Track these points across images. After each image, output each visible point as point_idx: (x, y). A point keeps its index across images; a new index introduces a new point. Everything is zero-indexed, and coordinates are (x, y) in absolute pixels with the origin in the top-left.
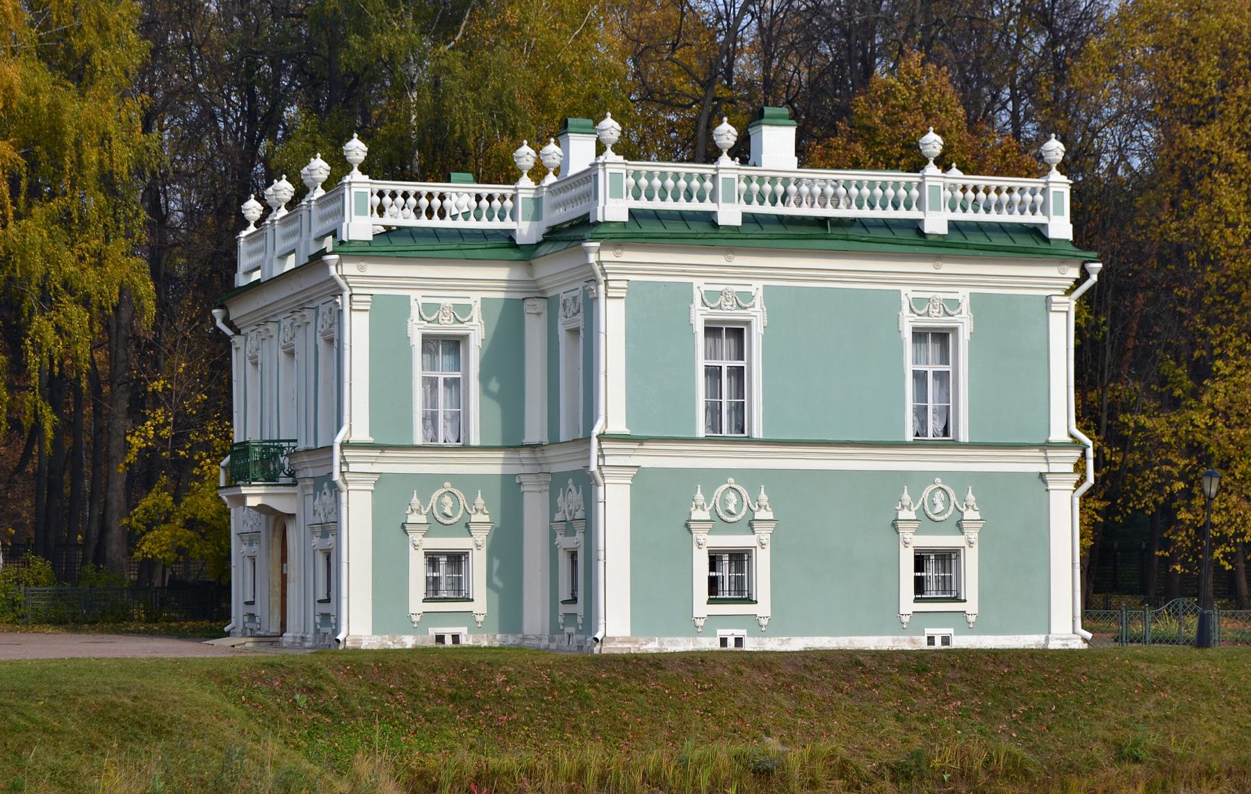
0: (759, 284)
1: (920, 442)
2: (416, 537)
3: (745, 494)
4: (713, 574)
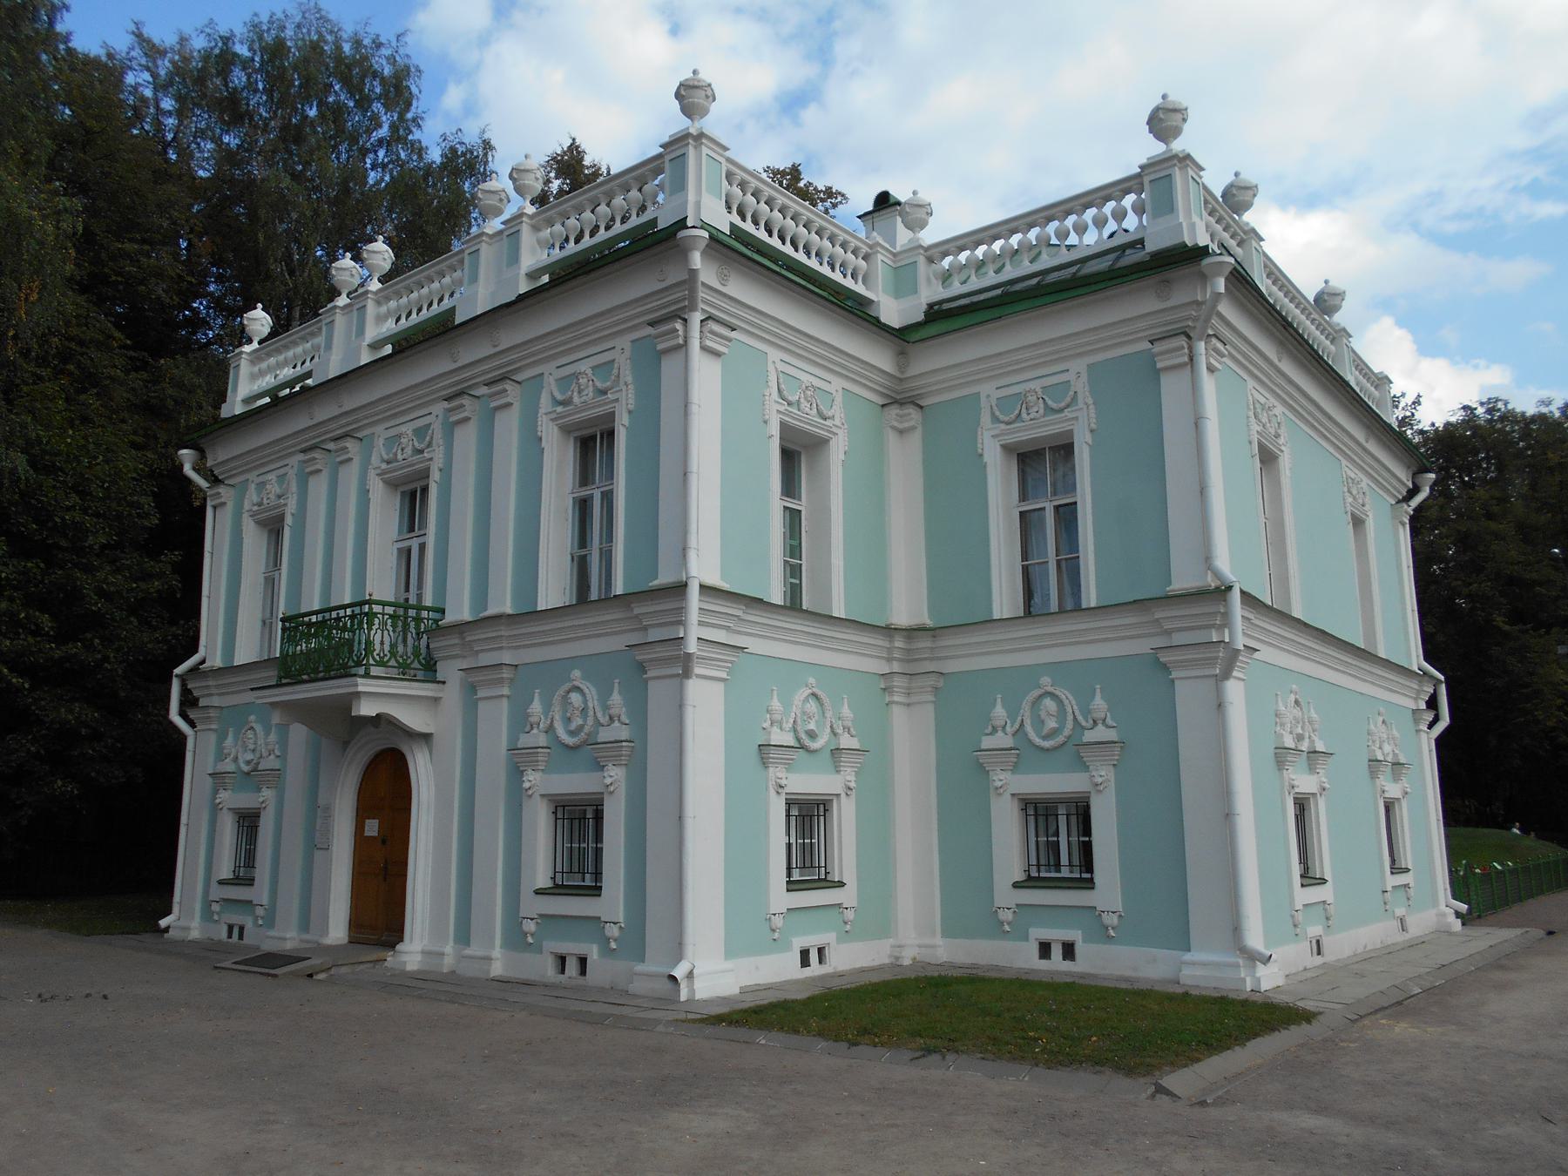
0: (1079, 365)
2: (1000, 777)
3: (826, 701)
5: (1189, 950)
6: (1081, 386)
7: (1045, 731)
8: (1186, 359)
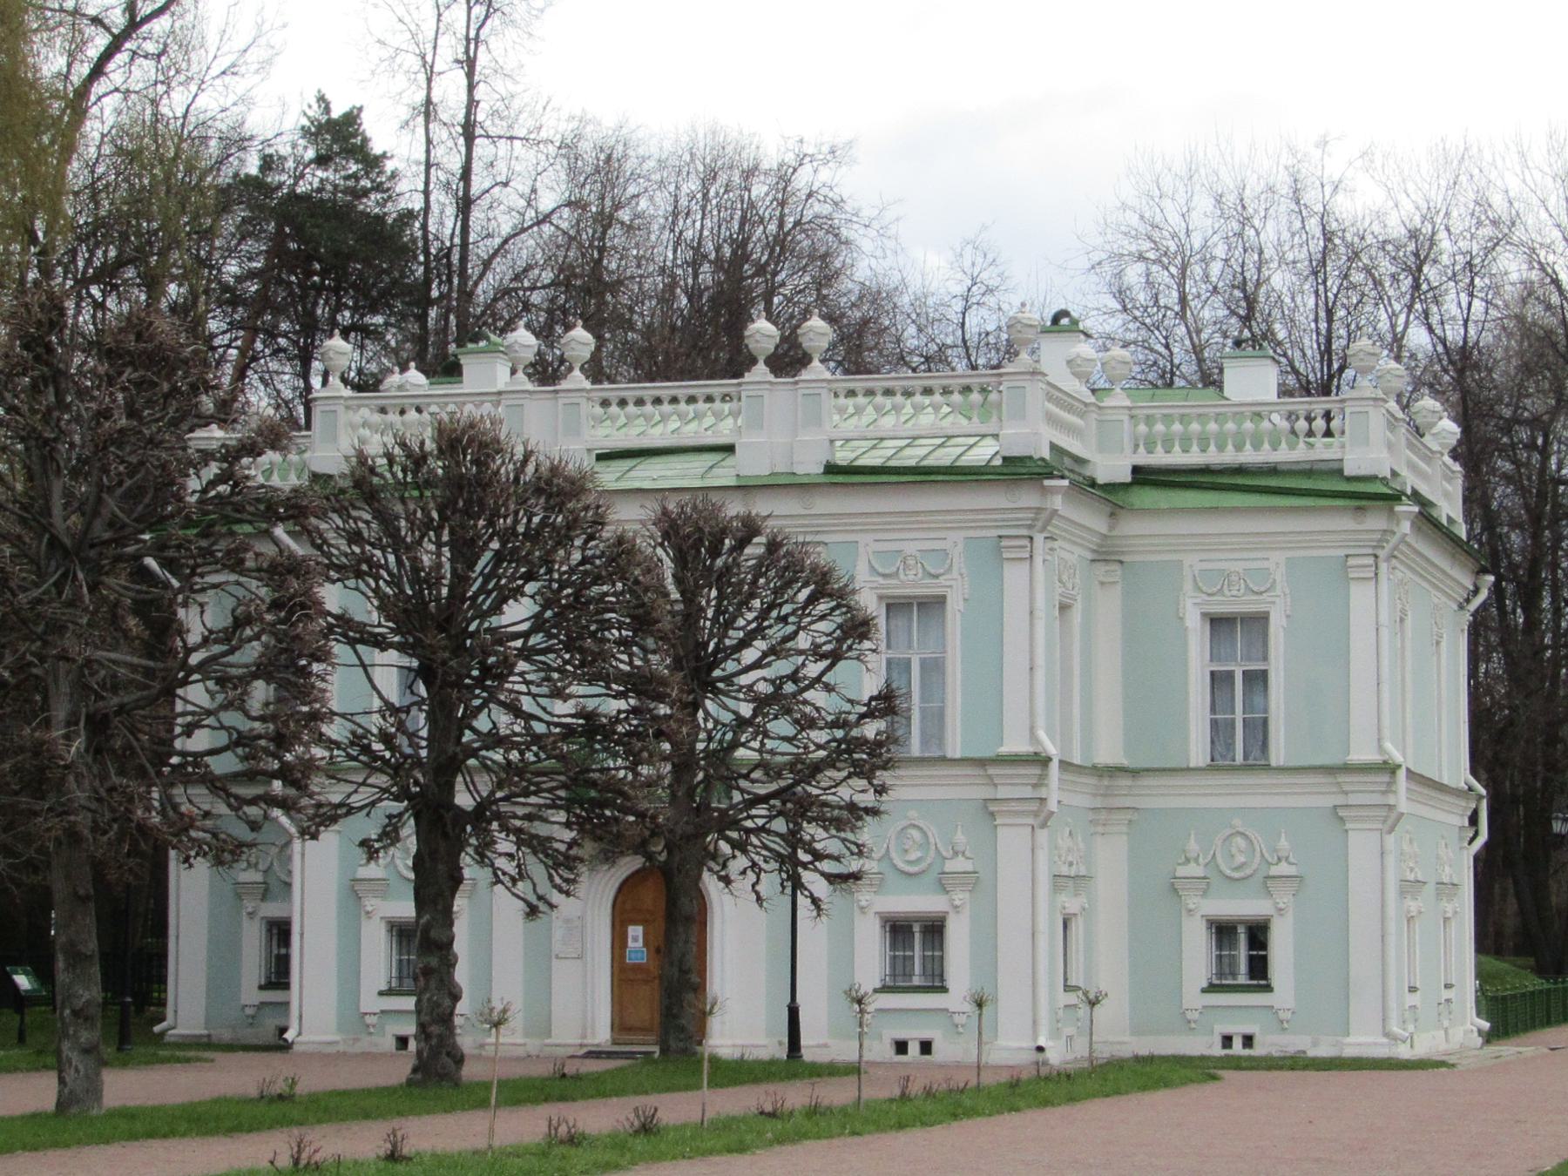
2: (1192, 901)
3: (933, 832)
5: (1348, 1035)
6: (1279, 576)
8: (1372, 575)
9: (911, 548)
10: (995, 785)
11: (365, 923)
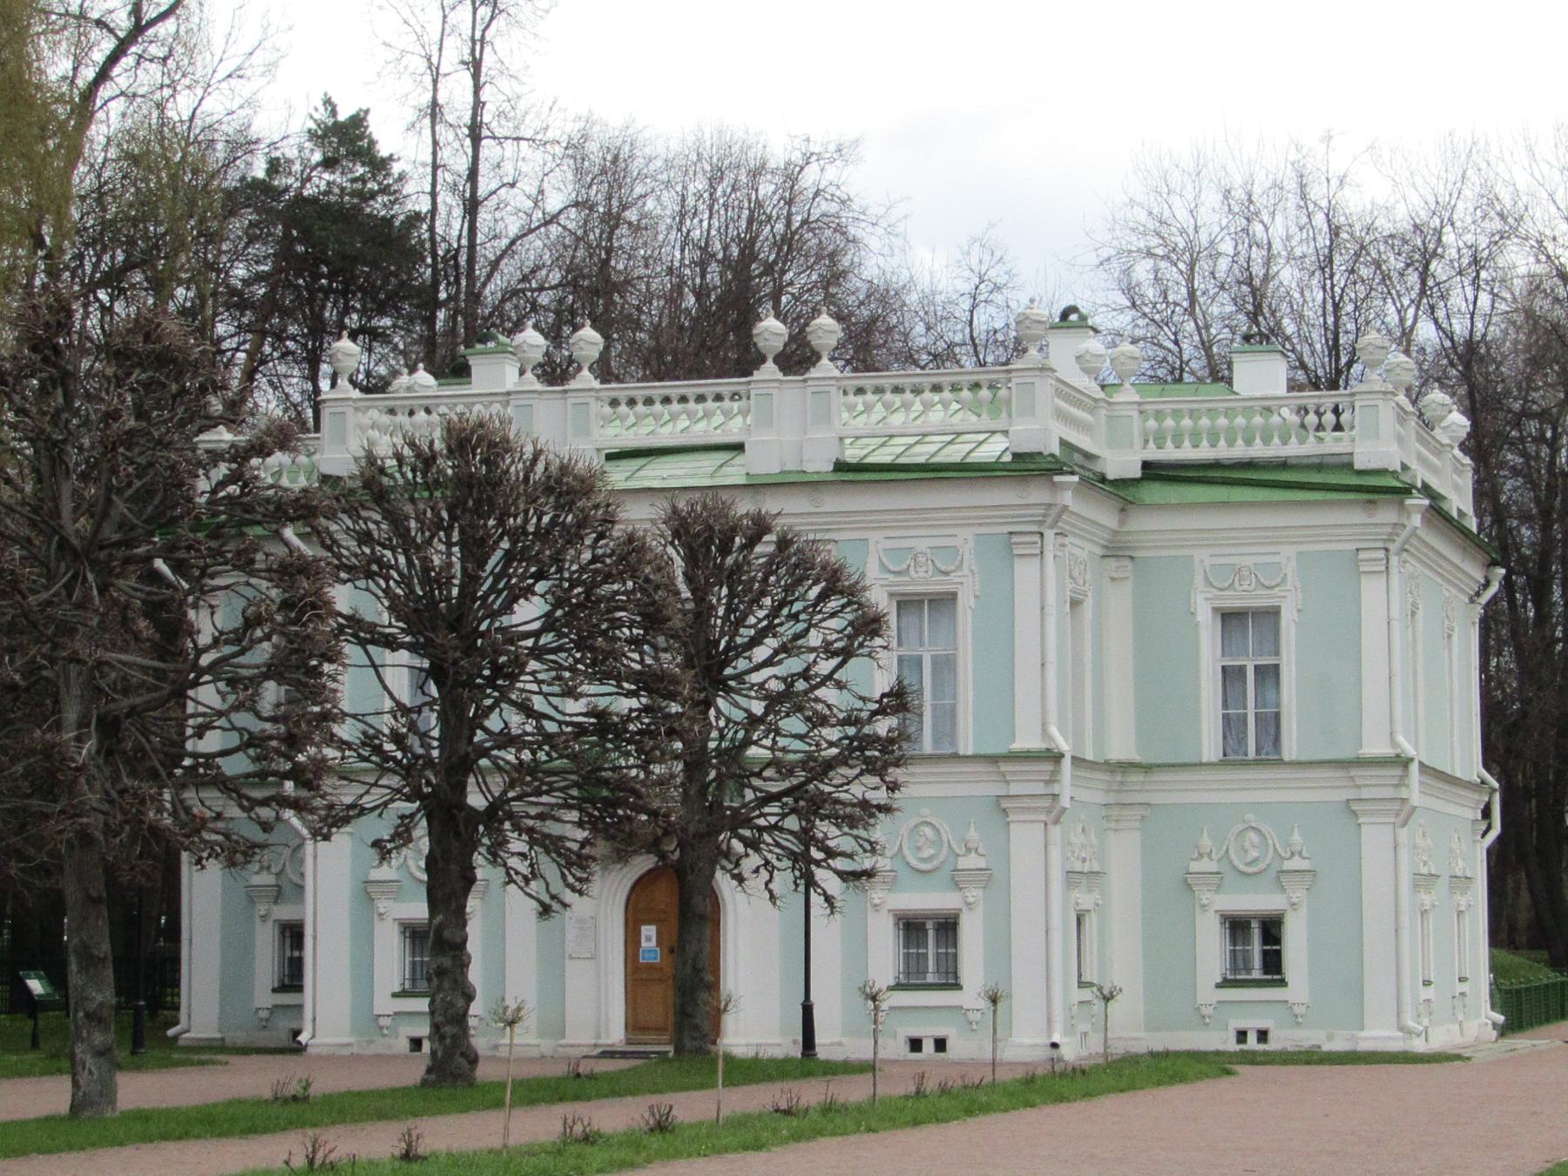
0: (968, 533)
1: (1232, 758)
2: (1205, 896)
3: (945, 828)
4: (296, 954)
6: (1290, 569)
7: (1249, 859)
9: (922, 545)
10: (1008, 782)
11: (872, 917)
